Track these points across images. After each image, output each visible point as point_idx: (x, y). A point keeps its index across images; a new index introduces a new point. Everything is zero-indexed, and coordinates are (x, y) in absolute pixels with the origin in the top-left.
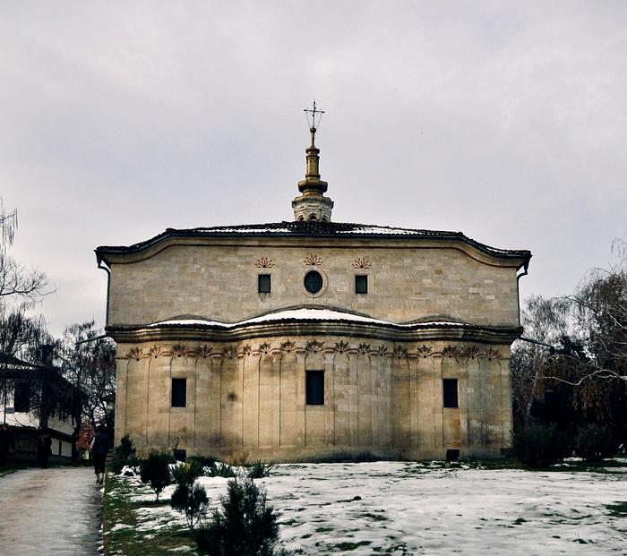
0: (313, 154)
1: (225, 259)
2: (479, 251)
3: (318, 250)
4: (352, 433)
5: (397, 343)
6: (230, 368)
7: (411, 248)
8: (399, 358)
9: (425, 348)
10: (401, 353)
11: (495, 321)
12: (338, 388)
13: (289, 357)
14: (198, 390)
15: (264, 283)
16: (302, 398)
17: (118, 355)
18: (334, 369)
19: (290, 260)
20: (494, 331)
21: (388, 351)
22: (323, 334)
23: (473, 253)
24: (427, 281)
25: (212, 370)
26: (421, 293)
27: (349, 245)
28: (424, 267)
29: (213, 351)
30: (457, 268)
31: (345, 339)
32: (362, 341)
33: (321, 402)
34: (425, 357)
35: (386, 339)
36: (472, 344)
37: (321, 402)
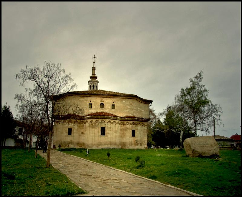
1: (82, 99)
9: (128, 123)
13: (97, 124)
14: (74, 131)
15: (90, 105)
16: (100, 134)
18: (107, 127)
22: (105, 119)
25: (78, 127)
31: (110, 120)
32: (114, 120)
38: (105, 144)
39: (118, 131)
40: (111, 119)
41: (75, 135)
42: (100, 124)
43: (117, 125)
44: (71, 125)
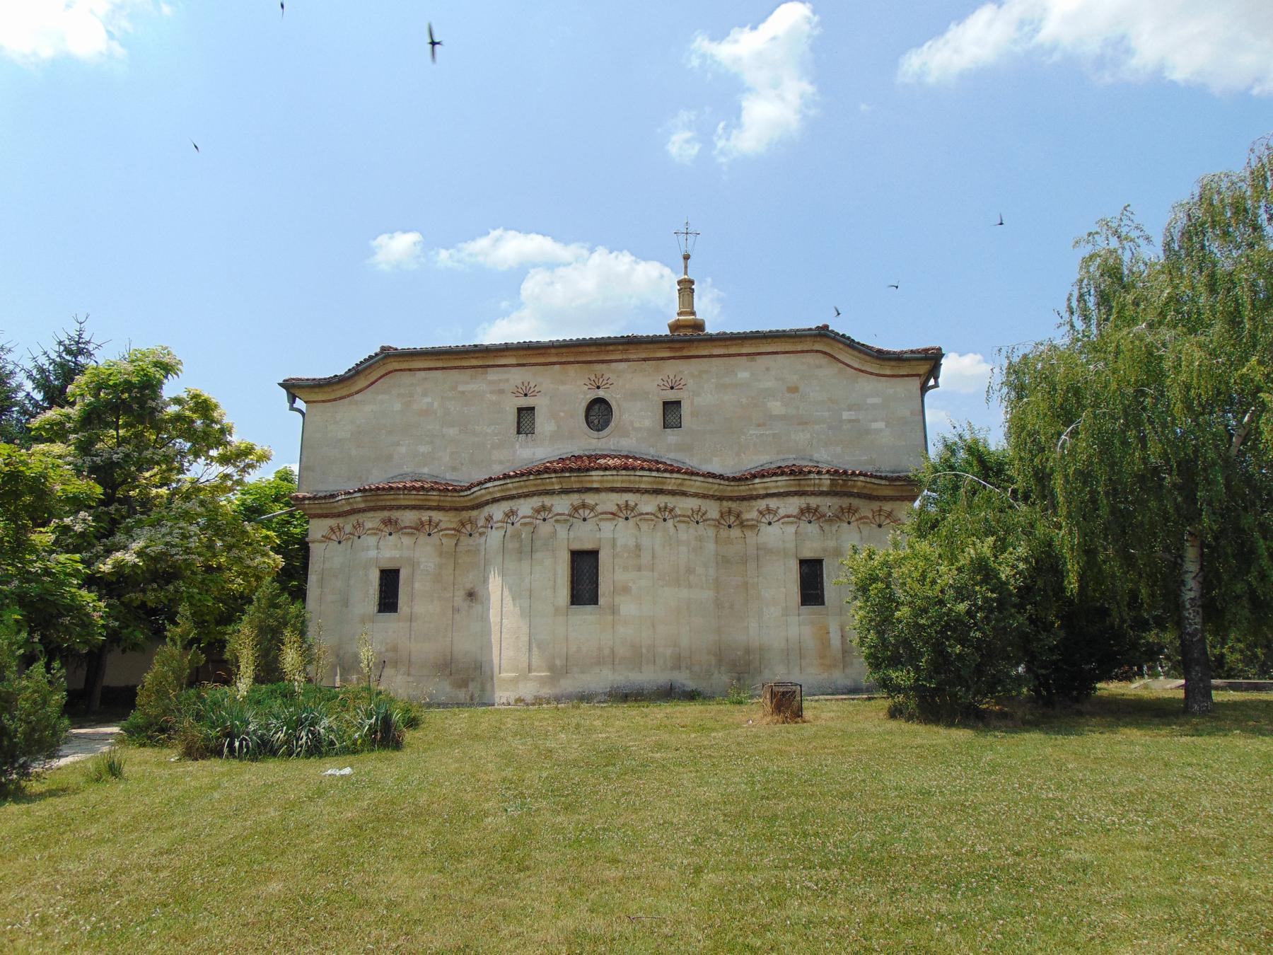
2: (856, 353)
3: (604, 366)
4: (644, 650)
5: (725, 503)
8: (730, 526)
9: (769, 510)
10: (732, 519)
11: (886, 465)
12: (620, 576)
14: (417, 585)
15: (525, 417)
16: (564, 593)
18: (614, 546)
19: (563, 383)
20: (885, 478)
21: (709, 516)
22: (597, 490)
24: (776, 407)
25: (441, 554)
26: (764, 425)
27: (652, 355)
28: (768, 384)
29: (443, 526)
30: (822, 380)
31: (631, 498)
32: (662, 500)
33: (594, 600)
34: (770, 524)
35: (705, 496)
36: (845, 502)
37: (594, 600)
38: (599, 662)
39: (700, 570)
40: (638, 491)
42: (562, 532)
43: (686, 533)
44: (387, 549)
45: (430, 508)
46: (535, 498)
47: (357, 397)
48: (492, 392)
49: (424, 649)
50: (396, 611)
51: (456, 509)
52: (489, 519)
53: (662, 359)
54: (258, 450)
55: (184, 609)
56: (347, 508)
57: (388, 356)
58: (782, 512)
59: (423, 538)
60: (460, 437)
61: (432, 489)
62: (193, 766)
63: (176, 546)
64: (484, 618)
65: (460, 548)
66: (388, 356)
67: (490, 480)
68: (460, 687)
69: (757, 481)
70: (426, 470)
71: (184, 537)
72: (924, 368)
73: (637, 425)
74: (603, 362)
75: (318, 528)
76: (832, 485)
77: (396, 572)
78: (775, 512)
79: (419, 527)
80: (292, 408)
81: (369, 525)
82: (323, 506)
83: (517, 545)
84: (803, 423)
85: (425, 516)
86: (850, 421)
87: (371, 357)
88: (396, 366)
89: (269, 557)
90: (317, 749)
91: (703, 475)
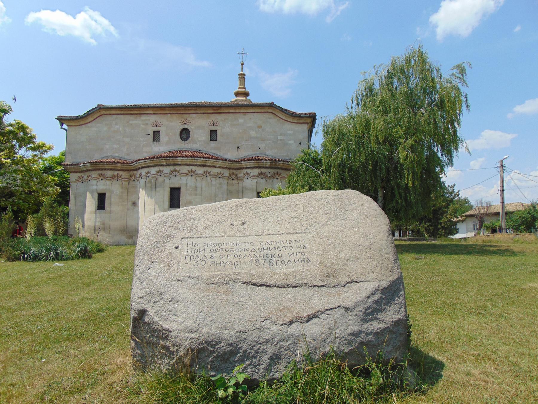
0: (242, 77)
1: (134, 122)
3: (187, 115)
5: (231, 170)
6: (133, 187)
7: (243, 113)
9: (247, 173)
10: (234, 176)
12: (189, 198)
13: (160, 179)
14: (113, 200)
15: (156, 135)
17: (71, 180)
21: (224, 175)
22: (180, 165)
23: (280, 115)
24: (253, 133)
25: (122, 188)
27: (206, 112)
29: (123, 177)
30: (271, 124)
31: (194, 168)
32: (205, 169)
35: (223, 168)
36: (276, 171)
40: (196, 165)
41: (114, 208)
42: (167, 180)
43: (215, 182)
44: (102, 186)
45: (117, 170)
46: (157, 167)
47: (89, 125)
48: (143, 124)
49: (116, 224)
50: (104, 209)
51: (128, 170)
52: (140, 175)
53: (210, 113)
54: (47, 145)
55: (9, 209)
56: (85, 169)
57: (100, 109)
58: (252, 174)
59: (115, 182)
60: (129, 141)
61: (118, 162)
62: (8, 263)
63: (12, 184)
64: (138, 213)
65: (129, 186)
66: (100, 109)
67: (140, 160)
68: (129, 238)
69: (243, 162)
70: (117, 155)
71: (15, 180)
72: (309, 120)
73: (200, 139)
74: (187, 114)
75: (73, 177)
76: (270, 165)
77: (104, 195)
78: (249, 174)
79: (113, 177)
80: (62, 128)
81: (93, 176)
82: (75, 168)
83: (150, 185)
84: (263, 140)
85: (116, 173)
86: (280, 140)
87: (94, 109)
88: (104, 112)
89: (54, 188)
90: (58, 257)
91: (222, 160)
